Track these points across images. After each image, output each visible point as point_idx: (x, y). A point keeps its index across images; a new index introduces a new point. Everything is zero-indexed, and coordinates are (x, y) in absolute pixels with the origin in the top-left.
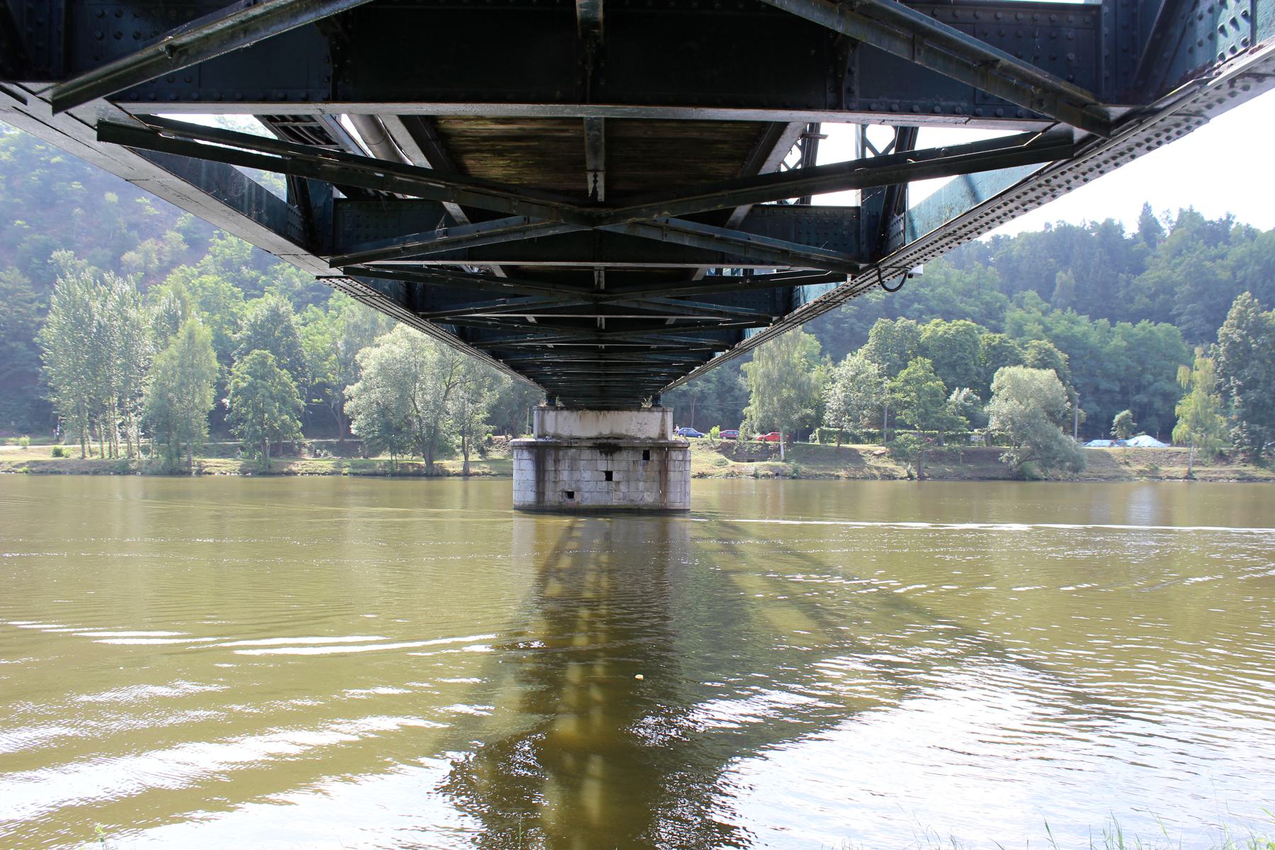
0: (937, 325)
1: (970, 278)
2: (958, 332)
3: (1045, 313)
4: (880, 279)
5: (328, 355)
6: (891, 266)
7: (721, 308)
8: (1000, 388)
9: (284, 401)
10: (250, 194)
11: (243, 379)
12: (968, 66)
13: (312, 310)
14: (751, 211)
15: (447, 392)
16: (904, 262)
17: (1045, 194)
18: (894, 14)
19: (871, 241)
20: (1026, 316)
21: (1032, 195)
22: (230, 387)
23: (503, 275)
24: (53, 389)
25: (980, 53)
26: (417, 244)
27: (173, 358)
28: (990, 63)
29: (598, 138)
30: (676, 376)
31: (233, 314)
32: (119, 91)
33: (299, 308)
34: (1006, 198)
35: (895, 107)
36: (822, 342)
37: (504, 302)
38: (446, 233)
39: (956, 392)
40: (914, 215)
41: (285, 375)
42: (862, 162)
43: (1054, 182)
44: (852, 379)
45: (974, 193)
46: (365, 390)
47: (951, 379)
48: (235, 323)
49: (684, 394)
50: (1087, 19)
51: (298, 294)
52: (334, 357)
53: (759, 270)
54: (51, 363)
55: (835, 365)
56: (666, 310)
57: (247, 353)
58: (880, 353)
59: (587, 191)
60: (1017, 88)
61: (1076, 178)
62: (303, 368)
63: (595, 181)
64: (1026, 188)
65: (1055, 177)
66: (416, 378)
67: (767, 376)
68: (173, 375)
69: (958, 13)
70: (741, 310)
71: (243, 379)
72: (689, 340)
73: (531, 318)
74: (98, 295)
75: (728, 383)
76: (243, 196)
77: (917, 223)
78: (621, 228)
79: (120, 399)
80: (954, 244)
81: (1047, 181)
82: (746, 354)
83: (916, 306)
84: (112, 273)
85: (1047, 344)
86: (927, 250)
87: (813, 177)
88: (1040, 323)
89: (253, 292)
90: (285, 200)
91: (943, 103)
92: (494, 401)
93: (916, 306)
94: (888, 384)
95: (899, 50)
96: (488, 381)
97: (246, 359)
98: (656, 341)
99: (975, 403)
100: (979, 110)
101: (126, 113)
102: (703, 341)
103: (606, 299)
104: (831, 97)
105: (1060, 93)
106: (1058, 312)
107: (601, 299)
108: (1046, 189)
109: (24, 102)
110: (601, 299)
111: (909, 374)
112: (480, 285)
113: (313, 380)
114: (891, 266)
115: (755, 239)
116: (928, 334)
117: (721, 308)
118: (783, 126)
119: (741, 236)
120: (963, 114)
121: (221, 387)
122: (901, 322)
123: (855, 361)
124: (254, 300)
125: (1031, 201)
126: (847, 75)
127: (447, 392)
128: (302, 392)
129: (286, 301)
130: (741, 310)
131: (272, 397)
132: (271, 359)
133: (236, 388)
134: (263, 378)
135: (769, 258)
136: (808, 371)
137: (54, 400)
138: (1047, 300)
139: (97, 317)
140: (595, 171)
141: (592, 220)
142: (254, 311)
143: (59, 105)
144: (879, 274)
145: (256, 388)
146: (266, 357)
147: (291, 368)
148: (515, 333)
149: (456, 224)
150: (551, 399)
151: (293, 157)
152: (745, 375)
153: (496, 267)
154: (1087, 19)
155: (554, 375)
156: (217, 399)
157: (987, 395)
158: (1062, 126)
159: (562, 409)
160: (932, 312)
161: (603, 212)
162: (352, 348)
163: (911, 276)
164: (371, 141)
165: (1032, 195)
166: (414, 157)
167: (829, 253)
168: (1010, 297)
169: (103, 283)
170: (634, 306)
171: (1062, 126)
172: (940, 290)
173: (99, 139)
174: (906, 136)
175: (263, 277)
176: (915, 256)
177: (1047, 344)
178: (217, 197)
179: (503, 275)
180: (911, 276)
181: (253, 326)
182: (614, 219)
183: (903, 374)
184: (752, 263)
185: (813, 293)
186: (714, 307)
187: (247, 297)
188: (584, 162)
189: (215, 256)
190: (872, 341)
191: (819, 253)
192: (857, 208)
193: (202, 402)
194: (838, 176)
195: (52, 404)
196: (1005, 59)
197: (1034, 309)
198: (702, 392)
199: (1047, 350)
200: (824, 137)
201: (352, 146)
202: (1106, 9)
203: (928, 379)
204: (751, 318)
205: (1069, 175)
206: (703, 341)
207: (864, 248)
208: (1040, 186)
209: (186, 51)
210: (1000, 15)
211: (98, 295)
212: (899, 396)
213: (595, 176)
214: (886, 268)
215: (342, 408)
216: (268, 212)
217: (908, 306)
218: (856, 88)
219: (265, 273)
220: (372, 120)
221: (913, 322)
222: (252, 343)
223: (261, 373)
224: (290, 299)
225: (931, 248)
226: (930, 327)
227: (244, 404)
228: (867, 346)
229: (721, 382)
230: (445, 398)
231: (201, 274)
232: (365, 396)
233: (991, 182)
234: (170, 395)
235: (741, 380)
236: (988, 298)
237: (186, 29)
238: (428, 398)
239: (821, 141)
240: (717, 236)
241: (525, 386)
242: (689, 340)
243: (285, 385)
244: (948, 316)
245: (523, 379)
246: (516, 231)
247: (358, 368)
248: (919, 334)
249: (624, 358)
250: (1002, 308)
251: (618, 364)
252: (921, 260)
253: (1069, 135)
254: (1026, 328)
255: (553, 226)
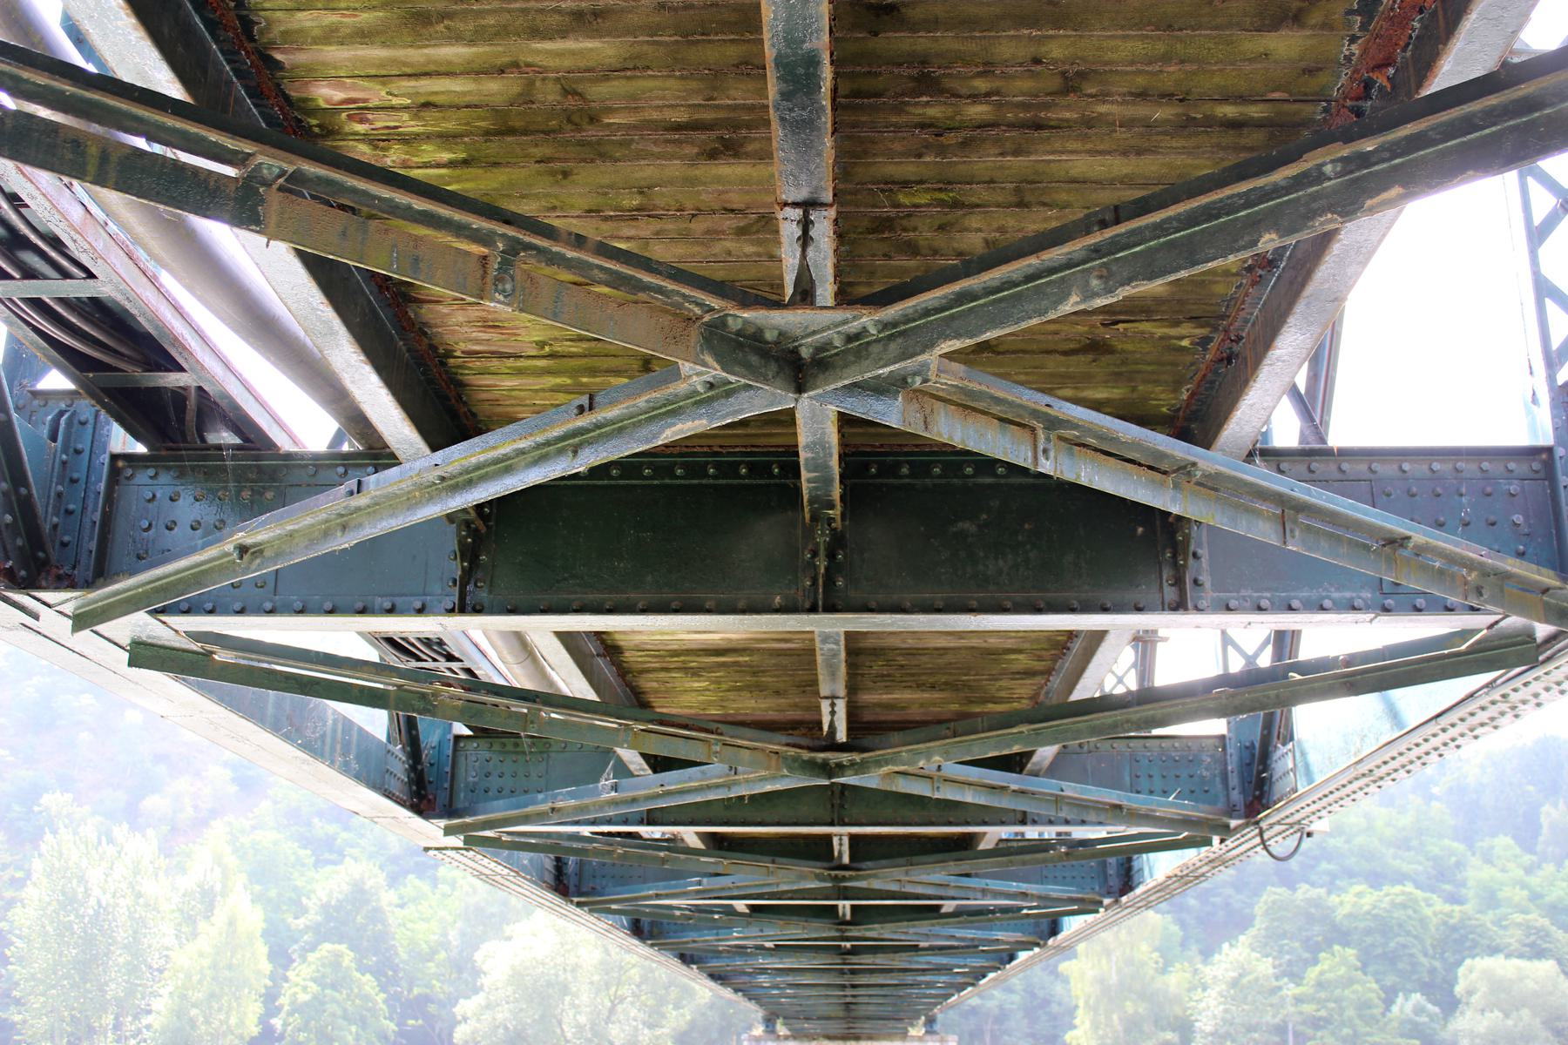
0: (1359, 895)
1: (1406, 820)
2: (1393, 904)
3: (1529, 870)
4: (1263, 842)
5: (434, 952)
6: (1279, 823)
7: (1024, 887)
8: (1470, 993)
9: (363, 1023)
10: (334, 731)
11: (305, 989)
12: (1366, 547)
13: (413, 883)
14: (1058, 755)
15: (612, 1010)
16: (1297, 817)
17: (1502, 714)
18: (1252, 485)
19: (1250, 787)
20: (1499, 875)
21: (1482, 716)
22: (284, 1001)
23: (699, 845)
24: (18, 1002)
25: (1381, 529)
26: (573, 802)
27: (201, 955)
28: (1395, 542)
29: (835, 655)
30: (961, 987)
31: (296, 889)
32: (164, 603)
33: (394, 880)
34: (1444, 721)
35: (1265, 603)
36: (1183, 925)
37: (699, 883)
38: (615, 788)
39: (1400, 1000)
40: (1307, 746)
41: (368, 983)
42: (1225, 680)
43: (1514, 697)
44: (1234, 983)
45: (1394, 715)
46: (488, 1007)
47: (1390, 980)
48: (298, 903)
49: (974, 1011)
50: (1536, 466)
51: (394, 860)
52: (442, 955)
53: (1079, 833)
54: (21, 960)
55: (1205, 962)
56: (941, 892)
57: (313, 948)
58: (1270, 942)
59: (820, 723)
60: (1441, 572)
61: (1547, 689)
62: (395, 972)
63: (833, 713)
64: (1472, 706)
65: (1515, 690)
66: (565, 989)
67: (1101, 981)
68: (200, 982)
69: (1345, 466)
70: (1054, 890)
71: (305, 989)
72: (979, 934)
73: (741, 905)
74: (102, 859)
75: (1041, 994)
76: (323, 736)
77: (1313, 758)
78: (871, 780)
79: (116, 1018)
80: (1373, 788)
81: (1504, 696)
82: (1067, 951)
83: (1324, 866)
84: (125, 826)
85: (1537, 919)
86: (1331, 798)
87: (1151, 703)
88: (1524, 886)
89: (327, 856)
90: (384, 738)
91: (1336, 595)
92: (683, 1026)
93: (1324, 866)
94: (1290, 990)
95: (1263, 531)
96: (674, 993)
97: (311, 957)
98: (927, 936)
99: (1431, 1016)
100: (1389, 602)
101: (175, 630)
102: (1000, 935)
103: (851, 879)
104: (1170, 594)
105: (1505, 576)
106: (1550, 868)
107: (844, 879)
108: (1504, 707)
109: (36, 617)
110: (844, 879)
111: (1322, 973)
112: (664, 861)
113: (410, 991)
114: (1279, 823)
115: (1071, 789)
116: (1346, 909)
117: (1024, 887)
118: (1098, 637)
119: (1048, 786)
120: (1365, 608)
121: (270, 999)
122: (1304, 892)
123: (1238, 956)
124: (330, 868)
125: (1482, 725)
126: (1191, 560)
127: (612, 1010)
128: (391, 1008)
129: (376, 870)
130: (1054, 890)
131: (345, 1017)
132: (348, 958)
133: (293, 1003)
134: (334, 986)
135: (1092, 817)
136: (1163, 971)
137: (17, 1018)
138: (1531, 851)
139: (96, 892)
140: (833, 697)
141: (827, 770)
142: (327, 886)
143: (82, 621)
144: (1261, 834)
145: (323, 1003)
146: (339, 955)
147: (377, 972)
148: (715, 926)
149: (631, 775)
150: (769, 1022)
151: (400, 687)
152: (1066, 981)
153: (690, 835)
154: (1536, 466)
155: (776, 987)
156: (264, 1021)
157: (1450, 1005)
158: (1514, 621)
159: (786, 1038)
160: (1351, 874)
161: (845, 757)
162: (472, 943)
163: (1309, 835)
164: (510, 659)
165: (1482, 716)
166: (572, 682)
167: (1183, 807)
168: (1471, 846)
169: (111, 841)
170: (894, 887)
171: (1514, 621)
172: (1359, 840)
173: (130, 665)
174: (1284, 641)
175: (344, 835)
176: (1313, 807)
177: (1537, 919)
178: (287, 738)
179: (699, 845)
180: (1309, 835)
181: (325, 908)
182: (860, 768)
183: (1312, 973)
184: (1067, 822)
185: (1159, 866)
186: (1015, 886)
187: (319, 863)
188: (814, 683)
189: (276, 803)
190: (1260, 924)
191: (1171, 805)
192: (1222, 737)
193: (241, 1023)
194: (1191, 699)
195: (13, 1025)
196: (1420, 535)
197: (1511, 866)
198: (1001, 1007)
199: (1539, 930)
200: (1165, 639)
201: (484, 664)
202: (1560, 452)
203: (1350, 982)
204: (1072, 901)
205: (1536, 687)
206: (1000, 935)
207: (1236, 796)
208: (1493, 703)
209: (261, 551)
210: (1406, 466)
211: (102, 859)
212: (1308, 1008)
213: (833, 705)
214: (1271, 826)
215: (451, 1035)
216: (358, 758)
217: (1313, 867)
218: (1205, 578)
219: (347, 828)
220: (519, 638)
221: (1322, 891)
222: (322, 934)
223: (332, 979)
224: (381, 868)
225: (1337, 795)
226: (1348, 898)
227: (305, 1027)
228: (1252, 931)
229: (1030, 992)
230: (608, 1020)
231: (254, 828)
232: (487, 1016)
233: (1419, 701)
234: (194, 1012)
235: (1059, 988)
236: (1436, 851)
237: (264, 523)
238: (582, 1019)
239: (1160, 646)
240: (1014, 787)
241: (730, 1002)
242: (979, 934)
243: (367, 998)
244: (1376, 879)
245: (727, 993)
246: (718, 786)
247: (477, 972)
248: (1333, 909)
249: (881, 960)
250: (1459, 865)
251: (872, 971)
252: (1324, 813)
253: (1530, 635)
254: (1501, 895)
255: (773, 778)
